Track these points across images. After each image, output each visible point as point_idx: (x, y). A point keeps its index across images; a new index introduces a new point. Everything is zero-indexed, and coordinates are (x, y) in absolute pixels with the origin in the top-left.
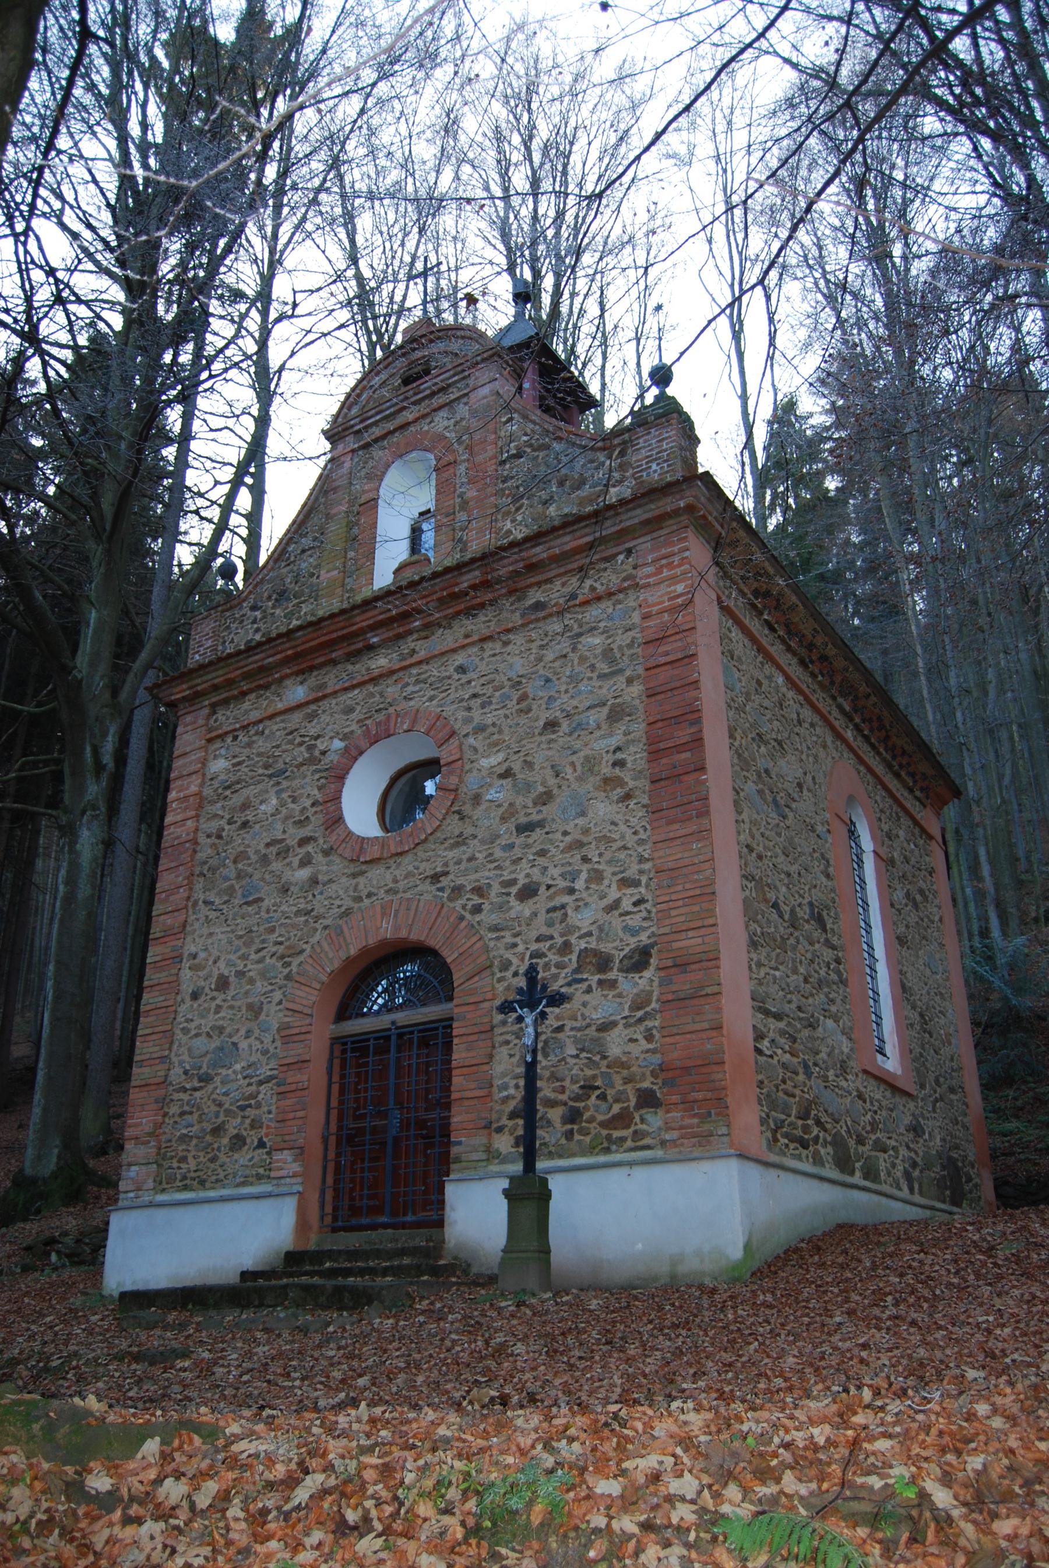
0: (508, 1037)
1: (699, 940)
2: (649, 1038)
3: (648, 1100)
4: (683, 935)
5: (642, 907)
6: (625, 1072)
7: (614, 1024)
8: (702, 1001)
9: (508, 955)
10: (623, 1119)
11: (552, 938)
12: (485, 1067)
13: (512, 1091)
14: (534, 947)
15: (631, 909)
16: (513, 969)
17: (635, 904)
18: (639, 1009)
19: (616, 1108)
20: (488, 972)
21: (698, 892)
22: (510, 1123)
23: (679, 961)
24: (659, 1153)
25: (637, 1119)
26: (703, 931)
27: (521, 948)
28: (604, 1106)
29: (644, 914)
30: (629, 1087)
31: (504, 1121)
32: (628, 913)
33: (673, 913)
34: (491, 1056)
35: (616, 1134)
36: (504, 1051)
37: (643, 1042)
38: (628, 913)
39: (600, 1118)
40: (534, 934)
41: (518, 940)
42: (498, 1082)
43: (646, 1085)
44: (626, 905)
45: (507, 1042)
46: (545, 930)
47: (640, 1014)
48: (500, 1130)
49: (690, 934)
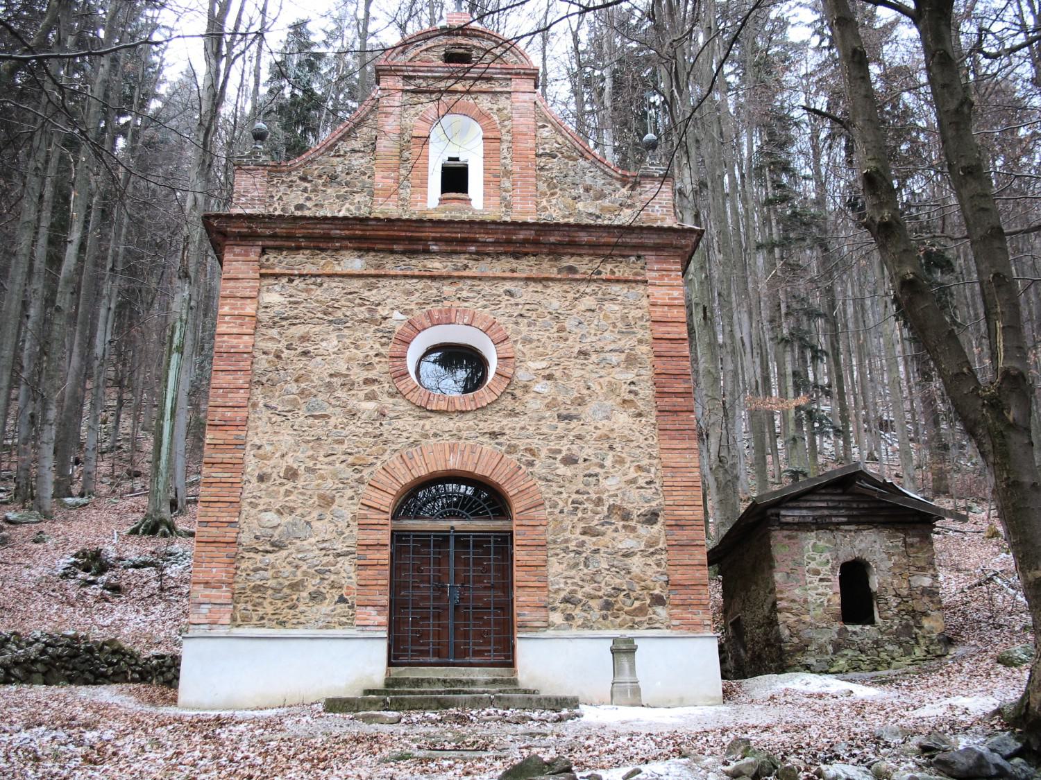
0: (558, 551)
1: (691, 513)
2: (659, 565)
3: (658, 601)
4: (681, 508)
5: (652, 486)
6: (642, 584)
7: (633, 554)
8: (694, 548)
9: (555, 498)
10: (641, 610)
11: (589, 493)
12: (542, 569)
13: (562, 586)
14: (574, 496)
15: (644, 485)
16: (560, 507)
17: (647, 483)
18: (651, 547)
19: (637, 604)
20: (542, 507)
21: (691, 484)
22: (562, 606)
23: (679, 523)
24: (667, 632)
25: (650, 611)
26: (694, 508)
27: (565, 496)
28: (629, 602)
29: (654, 490)
30: (645, 592)
31: (557, 604)
32: (642, 488)
33: (674, 493)
34: (546, 561)
35: (637, 619)
36: (553, 560)
37: (655, 567)
38: (642, 488)
39: (626, 608)
40: (575, 488)
41: (562, 490)
42: (551, 578)
43: (657, 592)
44: (641, 482)
45: (557, 555)
46: (581, 486)
47: (652, 550)
48: (554, 609)
49: (686, 508)
